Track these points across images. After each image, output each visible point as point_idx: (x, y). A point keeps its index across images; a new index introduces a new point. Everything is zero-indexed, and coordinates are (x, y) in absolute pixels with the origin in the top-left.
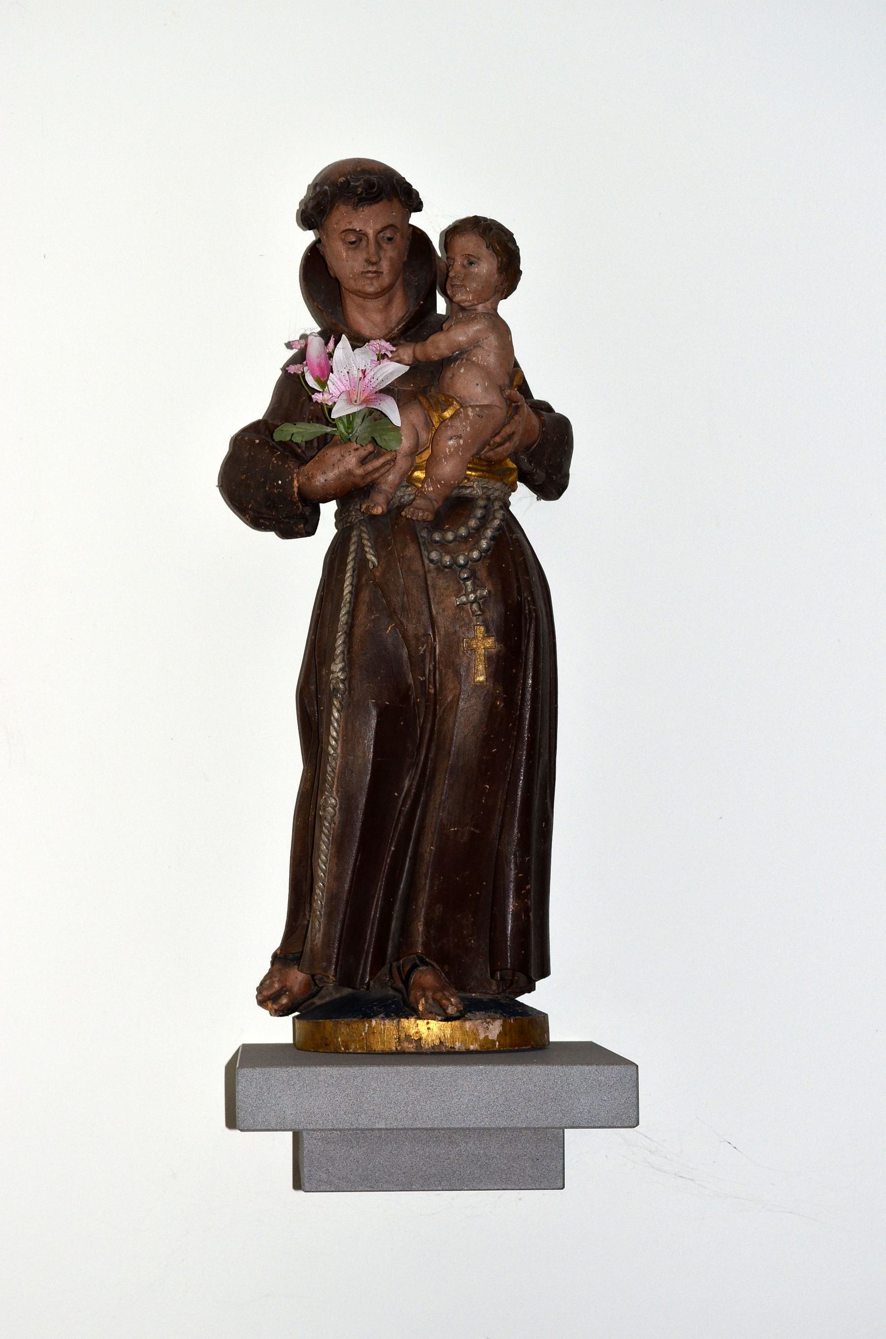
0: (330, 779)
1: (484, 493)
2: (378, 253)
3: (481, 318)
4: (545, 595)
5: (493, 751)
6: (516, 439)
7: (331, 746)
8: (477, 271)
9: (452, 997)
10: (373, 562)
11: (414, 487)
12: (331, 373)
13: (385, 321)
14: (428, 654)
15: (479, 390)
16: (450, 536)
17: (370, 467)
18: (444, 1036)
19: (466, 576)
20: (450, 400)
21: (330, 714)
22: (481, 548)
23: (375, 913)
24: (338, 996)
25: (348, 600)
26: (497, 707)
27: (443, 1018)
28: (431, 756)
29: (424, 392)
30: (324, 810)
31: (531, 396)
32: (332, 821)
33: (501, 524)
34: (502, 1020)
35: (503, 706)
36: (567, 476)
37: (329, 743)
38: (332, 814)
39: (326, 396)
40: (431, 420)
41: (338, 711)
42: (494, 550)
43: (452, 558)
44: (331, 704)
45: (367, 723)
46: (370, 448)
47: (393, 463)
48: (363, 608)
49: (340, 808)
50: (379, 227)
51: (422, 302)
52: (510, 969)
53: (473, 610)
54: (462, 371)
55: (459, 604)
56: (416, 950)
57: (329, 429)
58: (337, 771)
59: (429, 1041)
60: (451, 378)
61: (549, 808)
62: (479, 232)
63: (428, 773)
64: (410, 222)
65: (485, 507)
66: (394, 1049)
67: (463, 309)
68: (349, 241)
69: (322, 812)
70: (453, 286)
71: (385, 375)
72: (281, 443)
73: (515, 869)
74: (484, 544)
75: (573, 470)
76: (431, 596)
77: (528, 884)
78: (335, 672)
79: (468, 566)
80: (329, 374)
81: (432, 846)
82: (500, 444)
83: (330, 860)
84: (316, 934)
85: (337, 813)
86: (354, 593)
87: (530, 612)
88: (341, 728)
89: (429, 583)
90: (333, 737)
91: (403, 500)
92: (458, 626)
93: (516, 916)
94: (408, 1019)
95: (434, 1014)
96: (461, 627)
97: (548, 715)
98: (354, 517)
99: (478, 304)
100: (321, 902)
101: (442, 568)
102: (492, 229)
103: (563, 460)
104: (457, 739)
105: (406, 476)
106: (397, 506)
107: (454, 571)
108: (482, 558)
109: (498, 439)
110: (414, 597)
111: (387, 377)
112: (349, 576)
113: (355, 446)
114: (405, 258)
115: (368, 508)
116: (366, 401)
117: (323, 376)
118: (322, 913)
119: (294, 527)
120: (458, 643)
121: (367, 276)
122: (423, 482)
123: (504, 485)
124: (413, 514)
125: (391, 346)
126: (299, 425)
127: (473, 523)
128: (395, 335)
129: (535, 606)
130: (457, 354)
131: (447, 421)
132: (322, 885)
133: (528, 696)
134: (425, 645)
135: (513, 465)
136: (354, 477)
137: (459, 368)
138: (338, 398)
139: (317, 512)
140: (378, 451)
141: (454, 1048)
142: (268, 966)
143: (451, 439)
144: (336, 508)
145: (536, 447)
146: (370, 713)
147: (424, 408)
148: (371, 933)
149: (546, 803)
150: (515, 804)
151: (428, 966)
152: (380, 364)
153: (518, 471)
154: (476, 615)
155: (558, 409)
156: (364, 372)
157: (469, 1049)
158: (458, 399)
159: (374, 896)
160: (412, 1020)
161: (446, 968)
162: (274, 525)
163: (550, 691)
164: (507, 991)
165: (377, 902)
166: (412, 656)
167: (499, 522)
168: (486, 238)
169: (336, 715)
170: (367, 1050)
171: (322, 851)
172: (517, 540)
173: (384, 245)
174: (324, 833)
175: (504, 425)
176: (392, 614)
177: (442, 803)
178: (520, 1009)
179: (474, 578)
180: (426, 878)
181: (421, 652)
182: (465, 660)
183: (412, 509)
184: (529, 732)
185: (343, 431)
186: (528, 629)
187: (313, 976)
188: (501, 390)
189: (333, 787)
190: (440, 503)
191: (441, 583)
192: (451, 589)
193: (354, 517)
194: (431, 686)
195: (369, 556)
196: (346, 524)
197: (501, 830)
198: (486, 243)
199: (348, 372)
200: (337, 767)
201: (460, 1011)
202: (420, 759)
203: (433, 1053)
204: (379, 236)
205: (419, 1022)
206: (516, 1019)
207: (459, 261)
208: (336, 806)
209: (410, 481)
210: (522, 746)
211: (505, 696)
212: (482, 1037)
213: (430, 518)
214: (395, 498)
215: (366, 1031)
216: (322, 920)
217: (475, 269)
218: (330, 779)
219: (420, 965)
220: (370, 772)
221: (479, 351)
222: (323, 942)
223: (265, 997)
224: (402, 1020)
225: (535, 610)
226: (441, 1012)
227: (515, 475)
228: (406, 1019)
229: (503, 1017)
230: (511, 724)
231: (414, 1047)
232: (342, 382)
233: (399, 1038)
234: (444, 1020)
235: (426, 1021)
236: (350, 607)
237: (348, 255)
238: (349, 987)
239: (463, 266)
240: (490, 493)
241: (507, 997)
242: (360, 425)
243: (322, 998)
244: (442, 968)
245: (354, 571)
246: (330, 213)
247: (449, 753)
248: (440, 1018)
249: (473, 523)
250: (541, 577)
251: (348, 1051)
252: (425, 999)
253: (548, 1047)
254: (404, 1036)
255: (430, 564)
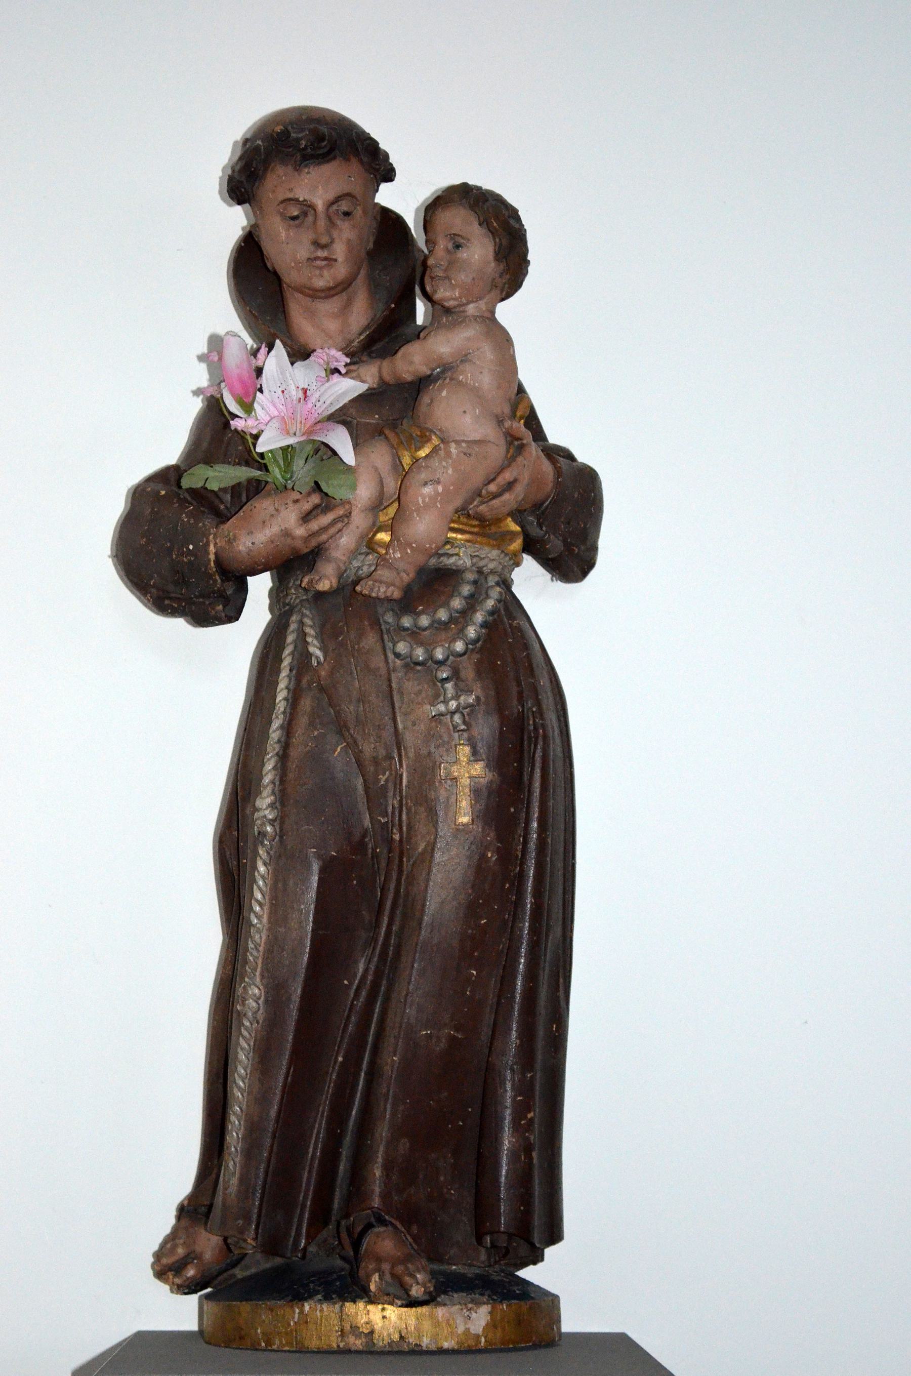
0: (252, 960)
1: (473, 565)
2: (328, 232)
3: (470, 320)
4: (559, 707)
5: (483, 922)
6: (519, 489)
7: (255, 913)
8: (466, 257)
9: (418, 1272)
10: (317, 657)
11: (376, 555)
12: (258, 393)
13: (342, 331)
14: (391, 785)
15: (468, 419)
16: (424, 621)
17: (314, 525)
18: (407, 1328)
19: (445, 676)
20: (427, 434)
21: (255, 868)
22: (466, 638)
23: (315, 1149)
24: (268, 1265)
25: (282, 709)
26: (488, 860)
27: (404, 1302)
28: (394, 928)
29: (394, 425)
30: (243, 1004)
31: (544, 439)
32: (254, 1020)
33: (496, 606)
34: (489, 1306)
35: (496, 859)
36: (594, 549)
37: (251, 909)
38: (254, 1010)
39: (251, 422)
40: (401, 463)
41: (265, 864)
42: (485, 642)
43: (427, 651)
44: (256, 854)
45: (306, 880)
46: (315, 499)
47: (346, 520)
48: (303, 721)
49: (266, 1001)
50: (331, 196)
51: (393, 306)
52: (504, 1233)
53: (454, 723)
54: (444, 393)
55: (435, 715)
56: (370, 1204)
57: (256, 473)
58: (261, 949)
59: (385, 1335)
60: (430, 405)
61: (563, 1003)
62: (469, 203)
63: (391, 953)
64: (376, 201)
65: (475, 582)
66: (335, 1345)
67: (448, 311)
68: (288, 215)
69: (240, 1005)
70: (432, 278)
71: (335, 396)
72: (191, 491)
73: (513, 1089)
74: (472, 632)
75: (602, 543)
76: (397, 705)
77: (530, 1112)
78: (261, 809)
79: (449, 662)
80: (256, 394)
81: (395, 1055)
82: (496, 496)
83: (250, 1073)
84: (229, 1179)
85: (261, 1008)
86: (291, 701)
87: (536, 729)
88: (268, 887)
89: (394, 685)
90: (257, 901)
91: (361, 572)
92: (433, 746)
93: (514, 1156)
94: (355, 1302)
95: (392, 1296)
96: (438, 747)
97: (561, 873)
98: (294, 596)
99: (468, 303)
100: (237, 1134)
101: (412, 665)
102: (487, 200)
103: (588, 526)
104: (432, 905)
105: (366, 539)
106: (352, 581)
107: (429, 670)
108: (468, 653)
109: (492, 488)
110: (373, 705)
111: (337, 400)
112: (284, 677)
113: (296, 496)
114: (371, 246)
115: (311, 582)
116: (309, 432)
117: (247, 394)
118: (238, 1149)
119: (210, 609)
120: (433, 771)
121: (316, 265)
122: (387, 546)
123: (502, 555)
124: (372, 590)
125: (344, 356)
126: (218, 467)
127: (457, 603)
128: (355, 349)
129: (542, 720)
130: (438, 373)
131: (421, 460)
132: (238, 1109)
133: (532, 846)
134: (387, 772)
135: (516, 528)
136: (293, 539)
137: (440, 390)
138: (267, 425)
139: (243, 589)
140: (327, 503)
141: (420, 1345)
142: (172, 1221)
143: (426, 484)
144: (269, 584)
145: (549, 504)
146: (309, 867)
147: (392, 447)
148: (308, 1178)
149: (559, 997)
150: (513, 997)
151: (386, 1225)
152: (328, 380)
153: (524, 538)
154: (458, 731)
155: (582, 457)
156: (305, 391)
157: (442, 1348)
158: (437, 433)
159: (313, 1127)
160: (361, 1305)
161: (415, 1230)
162: (184, 607)
163: (565, 840)
164: (502, 1262)
165: (318, 1133)
166: (369, 788)
167: (493, 603)
168: (479, 213)
169: (262, 869)
170: (296, 1347)
171: (240, 1062)
172: (519, 629)
173: (339, 222)
174: (243, 1037)
175: (501, 470)
176: (341, 728)
177: (410, 995)
178: (518, 1290)
179: (457, 679)
180: (386, 1101)
181: (382, 783)
182: (443, 794)
183: (370, 583)
184: (534, 896)
185: (279, 476)
186: (532, 751)
187: (225, 1240)
188: (500, 422)
189: (256, 971)
190: (412, 575)
191: (411, 686)
192: (424, 695)
193: (294, 596)
194: (395, 831)
195: (311, 649)
196: (284, 607)
197: (494, 1031)
198: (479, 218)
199: (283, 392)
200: (262, 943)
201: (430, 1293)
202: (379, 933)
203: (389, 1353)
204: (331, 210)
205: (371, 1307)
206: (510, 1305)
207: (442, 244)
208: (259, 998)
209: (371, 545)
210: (522, 917)
211: (499, 845)
212: (461, 1329)
213: (397, 594)
214: (351, 569)
215: (296, 1320)
216: (238, 1160)
217: (463, 254)
218: (252, 960)
219: (375, 1223)
220: (307, 951)
221: (467, 367)
222: (239, 1191)
223: (165, 1266)
224: (347, 1304)
225: (544, 726)
226: (401, 1293)
227: (517, 544)
228: (352, 1303)
229: (491, 1301)
230: (507, 885)
231: (364, 1344)
232: (275, 407)
233: (342, 1331)
234: (407, 1306)
235: (380, 1307)
236: (284, 720)
237: (288, 236)
238: (278, 1255)
239: (448, 251)
240: (481, 564)
241: (503, 1271)
242: (303, 468)
243: (247, 1268)
244: (409, 1232)
245: (291, 670)
246: (263, 177)
247: (420, 924)
248: (399, 1302)
249: (457, 603)
250: (554, 682)
251: (270, 1348)
252: (380, 1275)
253: (559, 1343)
254: (349, 1328)
255: (397, 660)
